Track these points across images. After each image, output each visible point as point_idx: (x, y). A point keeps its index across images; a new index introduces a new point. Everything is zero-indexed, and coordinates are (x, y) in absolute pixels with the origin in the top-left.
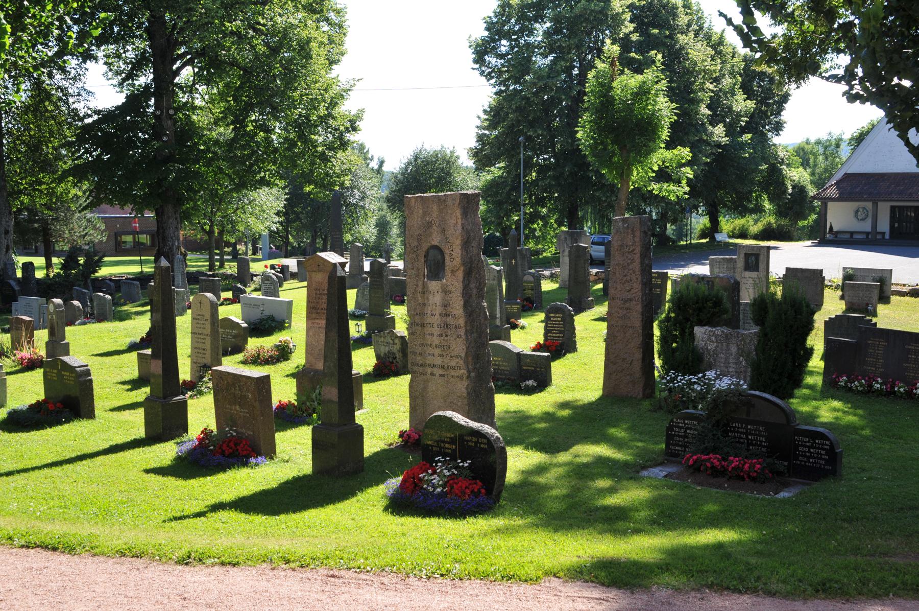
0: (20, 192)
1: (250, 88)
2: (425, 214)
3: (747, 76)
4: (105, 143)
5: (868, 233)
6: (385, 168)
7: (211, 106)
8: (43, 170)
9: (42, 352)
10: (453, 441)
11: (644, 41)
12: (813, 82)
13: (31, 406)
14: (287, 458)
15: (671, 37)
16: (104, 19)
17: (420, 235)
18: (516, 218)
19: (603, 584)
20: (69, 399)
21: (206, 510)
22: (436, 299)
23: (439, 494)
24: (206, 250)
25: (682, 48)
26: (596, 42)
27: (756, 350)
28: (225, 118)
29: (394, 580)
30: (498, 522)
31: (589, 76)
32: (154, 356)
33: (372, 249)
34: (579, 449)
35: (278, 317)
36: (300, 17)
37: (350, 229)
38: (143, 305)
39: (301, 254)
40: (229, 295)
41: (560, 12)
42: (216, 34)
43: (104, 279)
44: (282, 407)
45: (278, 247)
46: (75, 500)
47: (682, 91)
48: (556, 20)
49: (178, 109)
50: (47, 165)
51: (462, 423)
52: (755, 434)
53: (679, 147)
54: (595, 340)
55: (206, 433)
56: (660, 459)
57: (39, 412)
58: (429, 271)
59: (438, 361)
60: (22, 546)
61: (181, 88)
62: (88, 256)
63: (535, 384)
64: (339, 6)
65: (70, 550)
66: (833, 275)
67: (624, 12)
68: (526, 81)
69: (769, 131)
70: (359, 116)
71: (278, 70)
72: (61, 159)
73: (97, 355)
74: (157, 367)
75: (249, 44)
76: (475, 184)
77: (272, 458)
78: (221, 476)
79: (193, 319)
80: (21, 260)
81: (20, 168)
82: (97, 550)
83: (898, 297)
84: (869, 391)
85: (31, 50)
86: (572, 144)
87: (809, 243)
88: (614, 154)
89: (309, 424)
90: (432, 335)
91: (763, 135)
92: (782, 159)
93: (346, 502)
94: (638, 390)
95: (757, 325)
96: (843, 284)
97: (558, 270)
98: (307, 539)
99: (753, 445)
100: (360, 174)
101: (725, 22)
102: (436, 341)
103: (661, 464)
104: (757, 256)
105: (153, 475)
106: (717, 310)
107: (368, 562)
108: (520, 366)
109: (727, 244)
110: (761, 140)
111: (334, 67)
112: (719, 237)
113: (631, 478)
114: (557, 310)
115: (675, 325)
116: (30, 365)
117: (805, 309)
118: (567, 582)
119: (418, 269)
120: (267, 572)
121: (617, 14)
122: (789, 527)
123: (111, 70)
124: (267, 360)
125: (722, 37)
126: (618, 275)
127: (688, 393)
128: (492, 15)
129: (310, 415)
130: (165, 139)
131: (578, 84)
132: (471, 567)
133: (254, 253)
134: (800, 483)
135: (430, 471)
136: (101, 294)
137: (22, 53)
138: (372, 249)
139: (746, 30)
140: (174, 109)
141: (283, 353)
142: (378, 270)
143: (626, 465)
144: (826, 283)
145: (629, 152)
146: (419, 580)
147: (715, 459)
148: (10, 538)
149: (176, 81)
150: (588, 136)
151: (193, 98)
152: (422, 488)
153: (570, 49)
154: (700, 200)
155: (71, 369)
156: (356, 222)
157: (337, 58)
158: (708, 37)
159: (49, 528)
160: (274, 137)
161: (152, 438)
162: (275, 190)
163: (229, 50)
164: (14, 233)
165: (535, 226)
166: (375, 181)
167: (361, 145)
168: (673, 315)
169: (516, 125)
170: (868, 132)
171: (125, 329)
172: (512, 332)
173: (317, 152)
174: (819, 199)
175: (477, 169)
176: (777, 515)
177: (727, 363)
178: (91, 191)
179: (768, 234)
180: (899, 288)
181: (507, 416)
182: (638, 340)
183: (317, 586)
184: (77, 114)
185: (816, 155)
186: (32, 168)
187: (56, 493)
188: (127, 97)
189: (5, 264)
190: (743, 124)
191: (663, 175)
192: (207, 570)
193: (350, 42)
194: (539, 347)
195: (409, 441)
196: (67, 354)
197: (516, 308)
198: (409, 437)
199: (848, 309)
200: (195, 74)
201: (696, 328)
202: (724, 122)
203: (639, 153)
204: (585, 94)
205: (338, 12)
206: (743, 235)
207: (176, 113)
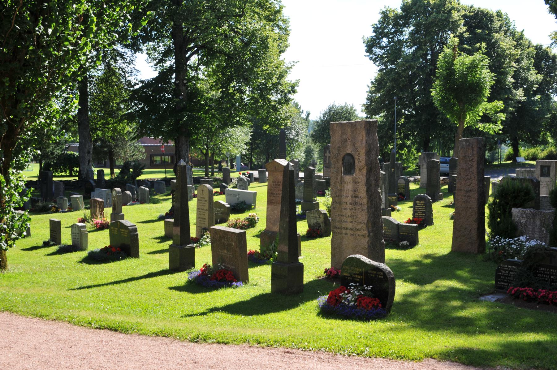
0: (97, 129)
1: (231, 67)
3: (538, 59)
6: (311, 118)
9: (108, 220)
10: (361, 274)
11: (472, 37)
13: (102, 249)
14: (255, 283)
15: (489, 34)
16: (149, 15)
17: (339, 147)
18: (391, 147)
19: (464, 364)
20: (124, 246)
22: (349, 187)
24: (203, 166)
25: (496, 41)
26: (441, 39)
27: (553, 223)
28: (216, 85)
29: (327, 356)
30: (391, 324)
31: (440, 57)
32: (175, 224)
34: (439, 282)
35: (248, 202)
36: (262, 24)
37: (289, 154)
38: (167, 195)
40: (218, 190)
44: (252, 254)
45: (245, 164)
46: (128, 303)
47: (497, 67)
48: (417, 25)
50: (111, 113)
51: (367, 262)
53: (496, 101)
54: (445, 219)
57: (107, 253)
59: (350, 225)
60: (97, 328)
61: (191, 67)
62: (135, 168)
63: (408, 244)
64: (285, 18)
65: (125, 331)
67: (459, 20)
68: (398, 63)
69: (552, 93)
70: (296, 84)
71: (248, 56)
73: (140, 222)
74: (177, 231)
77: (246, 283)
82: (141, 332)
85: (107, 35)
88: (455, 105)
89: (268, 264)
90: (346, 209)
93: (293, 310)
95: (554, 207)
97: (419, 177)
98: (271, 330)
100: (295, 120)
102: (349, 213)
105: (174, 291)
106: (527, 198)
107: (310, 345)
108: (398, 232)
111: (282, 54)
112: (519, 160)
113: (474, 301)
115: (499, 207)
116: (102, 227)
118: (440, 361)
121: (455, 21)
123: (150, 58)
124: (241, 227)
128: (377, 23)
129: (269, 259)
132: (376, 350)
133: (232, 167)
135: (346, 292)
136: (143, 187)
140: (186, 79)
141: (251, 223)
143: (470, 293)
146: (343, 357)
147: (529, 291)
148: (90, 323)
149: (188, 63)
150: (438, 94)
151: (198, 74)
152: (341, 302)
153: (426, 43)
155: (126, 227)
157: (283, 49)
158: (513, 34)
160: (245, 97)
161: (174, 269)
163: (220, 44)
164: (93, 153)
165: (403, 152)
166: (305, 125)
167: (296, 104)
169: (390, 90)
172: (392, 213)
173: (271, 105)
177: (533, 231)
178: (138, 129)
181: (391, 262)
183: (278, 358)
184: (130, 84)
188: (159, 73)
189: (88, 171)
191: (486, 119)
192: (209, 346)
193: (291, 40)
194: (409, 221)
195: (331, 275)
197: (394, 198)
198: (331, 273)
200: (199, 60)
201: (513, 209)
202: (523, 87)
205: (284, 21)
207: (187, 83)
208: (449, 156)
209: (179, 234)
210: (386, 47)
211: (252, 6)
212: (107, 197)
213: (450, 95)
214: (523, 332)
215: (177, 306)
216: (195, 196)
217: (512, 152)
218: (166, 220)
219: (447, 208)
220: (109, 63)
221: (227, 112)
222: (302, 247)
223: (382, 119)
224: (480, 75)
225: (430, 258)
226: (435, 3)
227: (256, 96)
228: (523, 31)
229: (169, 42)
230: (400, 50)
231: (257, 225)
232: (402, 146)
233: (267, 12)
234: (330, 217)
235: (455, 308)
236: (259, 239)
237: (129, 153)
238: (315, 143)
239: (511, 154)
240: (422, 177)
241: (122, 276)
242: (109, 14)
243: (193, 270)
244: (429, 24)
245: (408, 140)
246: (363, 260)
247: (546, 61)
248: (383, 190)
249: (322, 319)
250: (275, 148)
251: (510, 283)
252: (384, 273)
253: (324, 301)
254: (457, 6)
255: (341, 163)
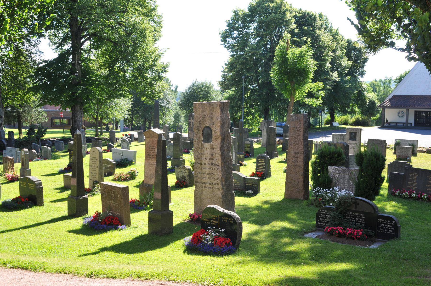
0: (8, 98)
1: (117, 51)
2: (203, 111)
3: (348, 49)
4: (48, 76)
5: (404, 123)
7: (98, 59)
8: (18, 88)
9: (18, 174)
10: (216, 219)
12: (384, 51)
14: (136, 226)
15: (313, 30)
16: (52, 17)
17: (200, 121)
18: (240, 114)
21: (99, 251)
23: (210, 244)
24: (94, 127)
26: (278, 33)
27: (358, 177)
28: (105, 65)
31: (277, 48)
32: (73, 176)
33: (172, 127)
35: (129, 159)
37: (162, 118)
39: (138, 129)
40: (106, 148)
41: (262, 18)
42: (102, 26)
43: (46, 140)
44: (133, 202)
45: (127, 126)
46: (35, 245)
47: (318, 57)
48: (260, 22)
49: (83, 61)
50: (20, 86)
52: (359, 218)
54: (279, 172)
55: (97, 213)
56: (314, 229)
57: (17, 202)
58: (205, 138)
59: (208, 181)
60: (11, 268)
61: (84, 51)
62: (40, 129)
63: (252, 192)
64: (159, 14)
65: (34, 270)
66: (390, 143)
67: (291, 19)
69: (358, 75)
70: (167, 66)
72: (27, 83)
74: (74, 182)
75: (117, 31)
76: (220, 98)
77: (129, 226)
78: (105, 235)
79: (91, 159)
80: (7, 130)
81: (8, 87)
82: (47, 270)
83: (421, 153)
84: (410, 198)
85: (17, 31)
86: (268, 79)
87: (377, 127)
88: (287, 85)
89: (145, 210)
91: (355, 77)
92: (364, 89)
93: (165, 248)
94: (301, 196)
96: (395, 147)
97: (261, 138)
98: (148, 266)
99: (358, 223)
100: (167, 92)
101: (350, 23)
102: (207, 171)
103: (314, 231)
104: (355, 133)
105: (72, 234)
108: (245, 184)
109: (338, 128)
110: (355, 79)
111: (156, 42)
112: (335, 124)
113: (300, 238)
114: (262, 157)
115: (319, 165)
116: (13, 180)
117: (381, 158)
119: (199, 137)
120: (130, 282)
122: (378, 263)
123: (51, 42)
124: (125, 179)
125: (337, 31)
126: (292, 141)
127: (325, 197)
128: (230, 19)
129: (146, 206)
130: (76, 74)
131: (270, 52)
133: (117, 129)
134: (381, 241)
136: (46, 147)
137: (12, 32)
138: (172, 127)
139: (360, 27)
140: (81, 60)
141: (132, 176)
142: (177, 138)
143: (298, 231)
144: (387, 146)
145: (294, 84)
147: (340, 229)
148: (5, 264)
149: (82, 47)
151: (90, 56)
152: (202, 241)
154: (326, 106)
155: (33, 182)
156: (164, 115)
157: (158, 38)
158: (331, 31)
159: (24, 259)
160: (127, 74)
161: (71, 216)
162: (127, 99)
165: (249, 118)
167: (167, 79)
168: (318, 160)
169: (239, 72)
170: (404, 77)
171: (57, 163)
172: (240, 167)
173: (147, 81)
174: (381, 107)
175: (221, 91)
176: (371, 256)
177: (344, 183)
178: (41, 98)
179: (357, 123)
180: (421, 149)
181: (240, 207)
182: (302, 172)
184: (35, 63)
185: (379, 87)
186: (13, 87)
187: (26, 242)
188: (59, 55)
190: (346, 72)
191: (310, 95)
193: (164, 31)
194: (253, 175)
196: (30, 175)
197: (242, 156)
198: (194, 217)
199: (399, 158)
200: (91, 45)
201: (329, 167)
202: (338, 70)
203: (299, 84)
204: (275, 56)
205: (159, 17)
206: (346, 123)
207: (82, 63)
208: (283, 122)
209: (76, 184)
210: (237, 38)
211: (134, 5)
212: (17, 155)
213: (284, 77)
214: (335, 262)
215: (75, 247)
216: (88, 153)
217: (330, 118)
218: (65, 174)
219: (282, 163)
220: (18, 46)
221: (113, 87)
222: (172, 195)
223: (233, 93)
224: (306, 62)
225: (268, 204)
226: (273, 6)
227: (136, 74)
228: (337, 29)
229: (67, 30)
230: (247, 41)
231: (137, 178)
232: (248, 114)
233: (145, 10)
234: (193, 171)
235: (286, 244)
236: (139, 189)
237: (34, 117)
238: (182, 110)
239: (329, 120)
240: (263, 138)
241: (30, 222)
242: (20, 14)
243: (87, 216)
244: (269, 21)
245: (253, 109)
246: (218, 209)
247: (355, 52)
248: (234, 154)
249: (187, 255)
250: (151, 114)
251: (327, 223)
252: (234, 219)
253: (189, 241)
254: (290, 8)
255: (202, 133)
